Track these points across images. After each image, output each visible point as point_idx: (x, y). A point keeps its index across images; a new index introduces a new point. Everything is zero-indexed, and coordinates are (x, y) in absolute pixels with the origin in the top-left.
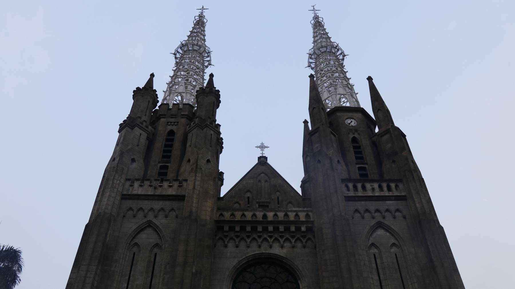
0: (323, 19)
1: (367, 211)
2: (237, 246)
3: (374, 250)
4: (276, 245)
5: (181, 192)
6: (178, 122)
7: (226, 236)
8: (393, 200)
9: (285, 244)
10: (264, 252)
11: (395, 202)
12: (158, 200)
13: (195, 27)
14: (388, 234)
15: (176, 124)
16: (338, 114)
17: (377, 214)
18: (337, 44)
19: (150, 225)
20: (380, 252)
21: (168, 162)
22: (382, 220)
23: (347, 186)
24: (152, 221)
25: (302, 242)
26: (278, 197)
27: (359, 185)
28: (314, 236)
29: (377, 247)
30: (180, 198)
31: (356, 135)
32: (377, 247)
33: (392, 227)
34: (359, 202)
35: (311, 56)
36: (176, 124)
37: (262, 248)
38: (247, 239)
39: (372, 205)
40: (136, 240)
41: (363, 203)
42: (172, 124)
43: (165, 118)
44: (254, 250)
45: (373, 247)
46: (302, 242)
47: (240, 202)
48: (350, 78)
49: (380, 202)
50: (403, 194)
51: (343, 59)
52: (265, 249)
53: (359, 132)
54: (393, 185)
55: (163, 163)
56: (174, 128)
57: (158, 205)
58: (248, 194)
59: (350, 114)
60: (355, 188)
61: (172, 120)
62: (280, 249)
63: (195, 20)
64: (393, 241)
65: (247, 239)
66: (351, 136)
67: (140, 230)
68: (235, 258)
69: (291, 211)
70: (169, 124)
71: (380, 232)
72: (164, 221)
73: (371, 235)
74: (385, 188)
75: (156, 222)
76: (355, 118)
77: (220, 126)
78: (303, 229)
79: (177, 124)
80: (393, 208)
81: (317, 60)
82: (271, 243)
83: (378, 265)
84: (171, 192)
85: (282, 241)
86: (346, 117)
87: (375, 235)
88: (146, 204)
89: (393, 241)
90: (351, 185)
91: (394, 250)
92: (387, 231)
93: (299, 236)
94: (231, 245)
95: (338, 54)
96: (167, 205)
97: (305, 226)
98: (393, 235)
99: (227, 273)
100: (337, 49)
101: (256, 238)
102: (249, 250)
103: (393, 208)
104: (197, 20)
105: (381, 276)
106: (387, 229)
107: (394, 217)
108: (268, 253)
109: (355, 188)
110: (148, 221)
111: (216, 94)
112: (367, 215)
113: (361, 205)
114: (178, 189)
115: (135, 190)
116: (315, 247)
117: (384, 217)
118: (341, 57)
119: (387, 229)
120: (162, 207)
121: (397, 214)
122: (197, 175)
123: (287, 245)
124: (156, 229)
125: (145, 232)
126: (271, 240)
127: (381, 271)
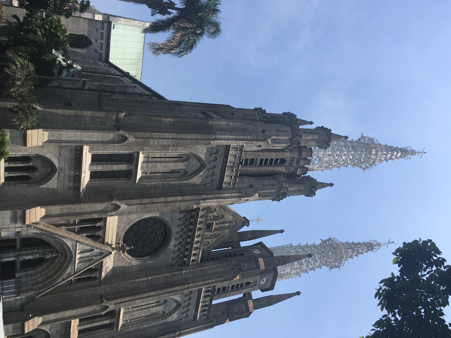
0: (411, 148)
1: (190, 298)
2: (179, 219)
6: (291, 166)
8: (195, 313)
11: (193, 314)
12: (222, 170)
14: (172, 309)
16: (272, 273)
18: (377, 165)
22: (182, 307)
24: (205, 167)
35: (370, 140)
37: (176, 234)
38: (183, 225)
41: (196, 296)
44: (175, 229)
48: (339, 169)
51: (361, 167)
52: (174, 235)
55: (203, 324)
57: (217, 171)
59: (270, 281)
62: (174, 245)
63: (407, 148)
65: (183, 225)
68: (171, 219)
76: (266, 284)
78: (185, 259)
79: (290, 162)
81: (365, 145)
86: (268, 278)
87: (173, 302)
88: (219, 162)
92: (174, 309)
93: (181, 256)
95: (367, 164)
97: (188, 260)
98: (171, 312)
100: (372, 164)
101: (184, 231)
103: (189, 313)
104: (407, 149)
107: (182, 314)
108: (172, 238)
110: (206, 165)
111: (311, 193)
117: (184, 308)
118: (363, 166)
120: (216, 174)
126: (181, 240)
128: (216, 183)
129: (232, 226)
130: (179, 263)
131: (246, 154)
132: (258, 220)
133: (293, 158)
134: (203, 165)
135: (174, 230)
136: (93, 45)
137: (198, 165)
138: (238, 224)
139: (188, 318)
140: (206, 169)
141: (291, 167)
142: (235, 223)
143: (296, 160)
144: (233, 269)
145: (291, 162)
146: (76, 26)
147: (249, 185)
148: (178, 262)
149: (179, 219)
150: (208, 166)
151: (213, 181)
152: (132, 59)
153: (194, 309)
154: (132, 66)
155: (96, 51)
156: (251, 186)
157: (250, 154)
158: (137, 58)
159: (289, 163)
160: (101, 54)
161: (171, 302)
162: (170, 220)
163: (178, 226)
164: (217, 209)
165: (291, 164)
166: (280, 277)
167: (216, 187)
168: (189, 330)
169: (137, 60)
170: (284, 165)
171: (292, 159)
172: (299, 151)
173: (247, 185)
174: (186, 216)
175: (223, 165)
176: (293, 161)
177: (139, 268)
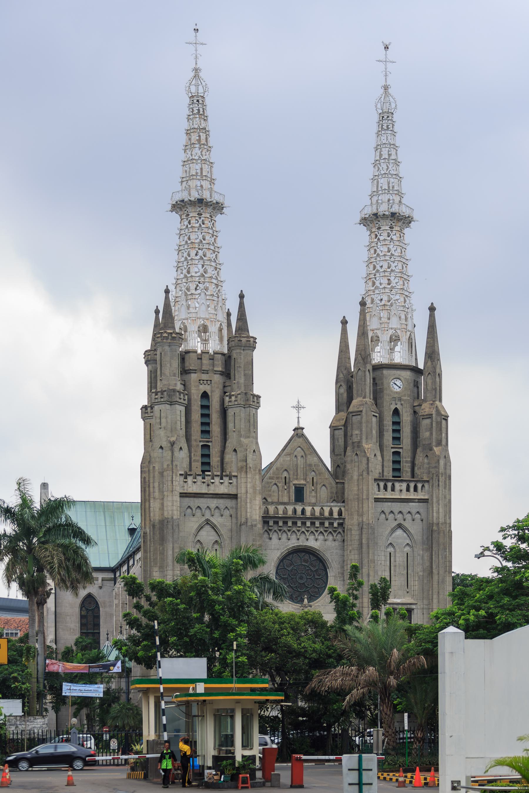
2: (280, 539)
3: (391, 549)
4: (312, 538)
5: (233, 491)
6: (211, 381)
7: (270, 530)
9: (319, 537)
10: (301, 544)
11: (417, 504)
13: (209, 179)
14: (405, 535)
15: (209, 382)
17: (400, 516)
19: (208, 522)
20: (395, 552)
21: (208, 442)
22: (402, 522)
23: (378, 485)
25: (333, 536)
26: (313, 478)
27: (389, 485)
28: (344, 531)
29: (394, 547)
30: (235, 497)
31: (399, 407)
32: (394, 547)
33: (409, 529)
34: (386, 503)
36: (209, 382)
37: (300, 540)
39: (396, 507)
40: (198, 538)
42: (205, 382)
43: (195, 373)
44: (294, 542)
45: (390, 547)
46: (333, 536)
47: (278, 485)
49: (405, 504)
50: (426, 497)
53: (402, 402)
54: (419, 486)
56: (207, 388)
57: (213, 503)
58: (285, 474)
60: (385, 488)
61: (204, 377)
64: (408, 541)
66: (393, 407)
67: (201, 528)
68: (278, 549)
69: (327, 506)
70: (202, 382)
71: (399, 532)
72: (220, 519)
73: (391, 535)
74: (412, 489)
75: (213, 520)
76: (402, 378)
77: (260, 397)
80: (414, 511)
82: (308, 537)
83: (392, 562)
84: (223, 489)
85: (316, 534)
87: (394, 535)
88: (203, 502)
89: (408, 541)
90: (382, 484)
91: (407, 549)
94: (274, 537)
96: (221, 503)
99: (273, 564)
101: (296, 531)
102: (290, 542)
105: (392, 572)
106: (405, 530)
109: (385, 488)
112: (391, 516)
113: (387, 507)
114: (229, 486)
115: (190, 487)
116: (344, 541)
119: (405, 530)
120: (217, 505)
121: (418, 516)
122: (248, 476)
123: (321, 537)
124: (214, 527)
125: (204, 529)
127: (392, 568)
128: (229, 503)
129: (303, 454)
130: (341, 532)
131: (194, 460)
132: (298, 407)
133: (200, 380)
134: (207, 523)
135: (294, 544)
136: (92, 592)
137: (208, 528)
138: (299, 444)
139: (421, 511)
140: (211, 519)
141: (213, 382)
142: (299, 449)
143: (203, 375)
144: (357, 454)
145: (205, 382)
146: (68, 617)
147: (234, 453)
148: (330, 532)
149: (280, 539)
150: (208, 516)
151: (226, 507)
152: (105, 523)
153: (410, 504)
154: (117, 524)
155: (101, 588)
156: (235, 450)
157: (194, 455)
158: (102, 513)
159: (207, 385)
160: (103, 580)
161: (394, 538)
162: (279, 551)
163: (289, 540)
164: (274, 482)
165: (209, 382)
166: (268, 514)
167: (234, 501)
168: (435, 511)
169: (106, 513)
170: (210, 394)
171: (202, 382)
172: (190, 373)
173: (234, 457)
174: (275, 531)
175: (206, 497)
176: (203, 380)
177: (339, 582)
